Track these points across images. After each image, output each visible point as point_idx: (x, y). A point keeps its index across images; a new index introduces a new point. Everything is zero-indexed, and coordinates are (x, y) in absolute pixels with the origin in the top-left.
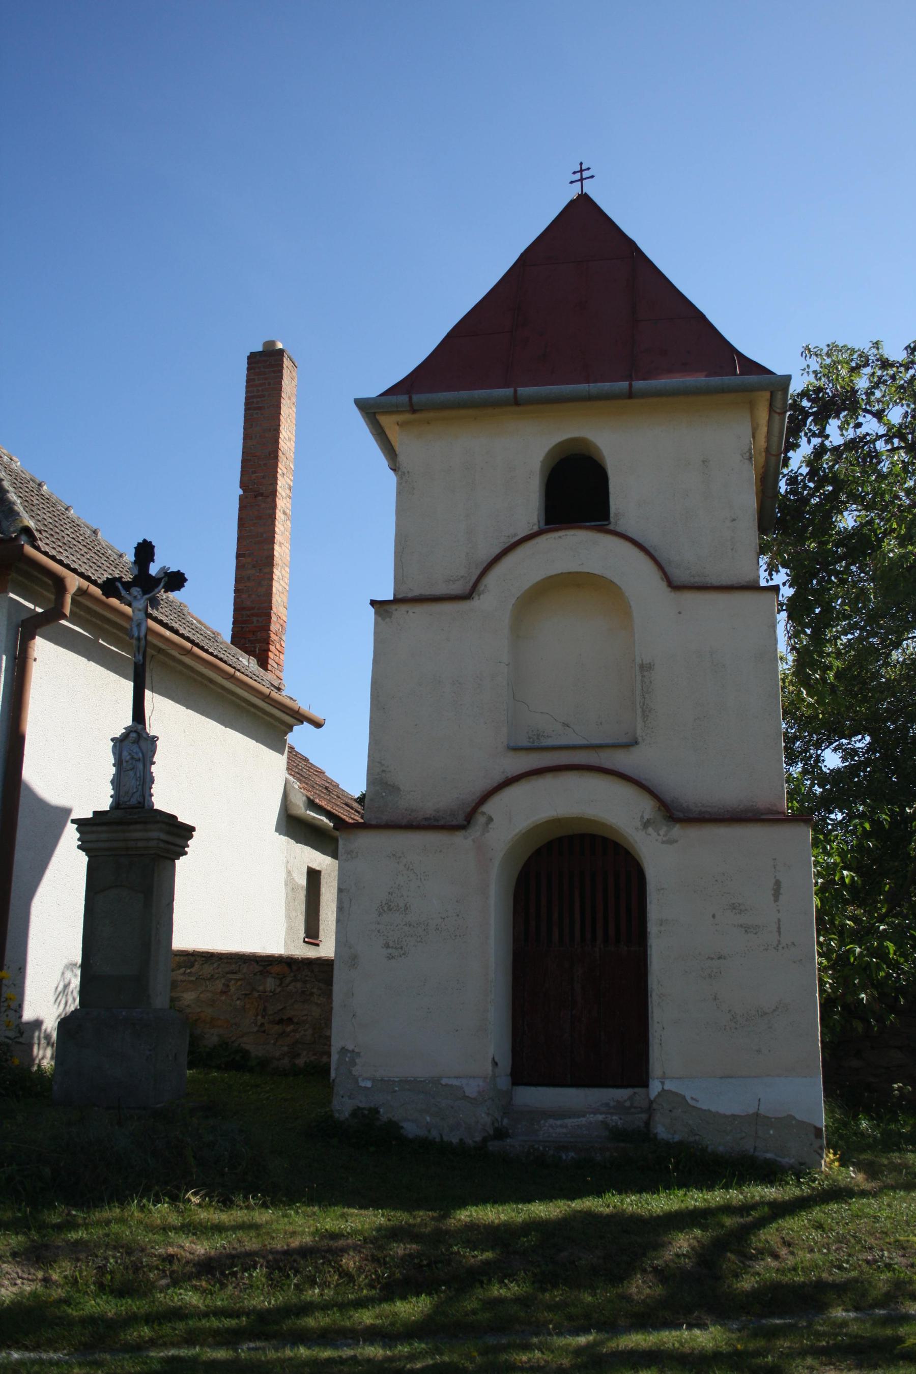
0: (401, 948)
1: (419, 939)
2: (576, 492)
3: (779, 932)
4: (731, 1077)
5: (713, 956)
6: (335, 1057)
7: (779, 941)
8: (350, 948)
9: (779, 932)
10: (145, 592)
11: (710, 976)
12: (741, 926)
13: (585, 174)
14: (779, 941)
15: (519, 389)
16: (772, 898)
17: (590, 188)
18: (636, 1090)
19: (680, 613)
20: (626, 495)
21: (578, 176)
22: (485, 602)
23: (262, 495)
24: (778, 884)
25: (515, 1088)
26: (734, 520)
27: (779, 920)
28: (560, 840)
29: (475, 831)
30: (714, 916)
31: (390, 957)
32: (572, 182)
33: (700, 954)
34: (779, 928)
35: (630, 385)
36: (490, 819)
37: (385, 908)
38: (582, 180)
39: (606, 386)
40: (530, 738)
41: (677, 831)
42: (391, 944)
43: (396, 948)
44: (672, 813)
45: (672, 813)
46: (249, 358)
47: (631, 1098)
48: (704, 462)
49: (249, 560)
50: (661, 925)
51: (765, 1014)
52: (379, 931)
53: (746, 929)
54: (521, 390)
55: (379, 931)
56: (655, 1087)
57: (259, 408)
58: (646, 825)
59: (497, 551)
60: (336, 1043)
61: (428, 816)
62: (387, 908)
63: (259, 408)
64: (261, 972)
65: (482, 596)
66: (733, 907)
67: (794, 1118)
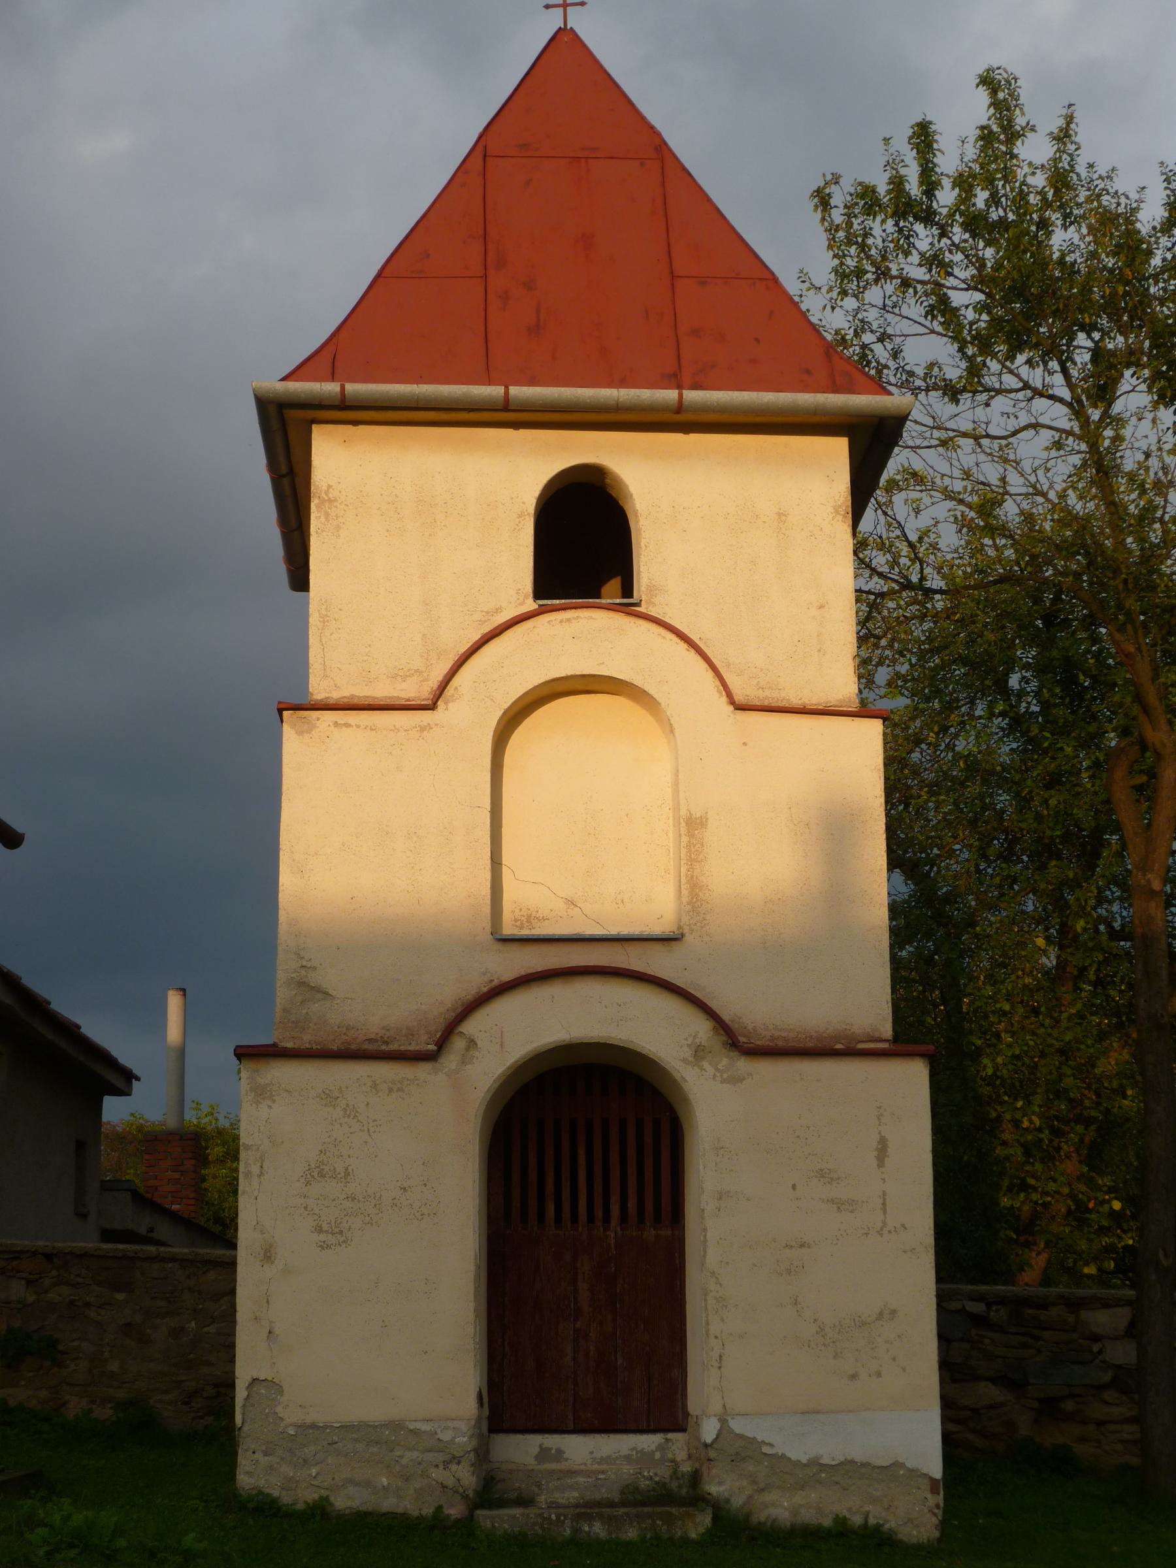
0: (341, 1232)
1: (368, 1219)
2: (583, 545)
3: (884, 1210)
4: (817, 1412)
5: (793, 1244)
6: (241, 1393)
7: (884, 1223)
8: (262, 1232)
9: (884, 1210)
11: (789, 1272)
12: (832, 1201)
14: (884, 1223)
15: (511, 388)
16: (875, 1162)
18: (670, 1436)
19: (745, 744)
20: (660, 554)
22: (447, 714)
25: (494, 1436)
26: (821, 607)
27: (884, 1193)
29: (450, 1060)
30: (794, 1187)
31: (324, 1246)
32: (547, 7)
33: (774, 1240)
34: (884, 1204)
35: (681, 396)
36: (472, 1043)
37: (315, 1174)
39: (645, 395)
40: (516, 920)
41: (744, 1064)
42: (325, 1227)
43: (333, 1234)
44: (737, 1041)
45: (737, 1041)
47: (661, 1448)
48: (779, 514)
50: (720, 1199)
51: (864, 1324)
52: (306, 1208)
53: (839, 1205)
54: (514, 391)
55: (306, 1208)
56: (709, 1430)
58: (699, 1053)
60: (244, 1373)
61: (372, 1036)
62: (318, 1172)
65: (450, 705)
66: (821, 1174)
67: (902, 1465)
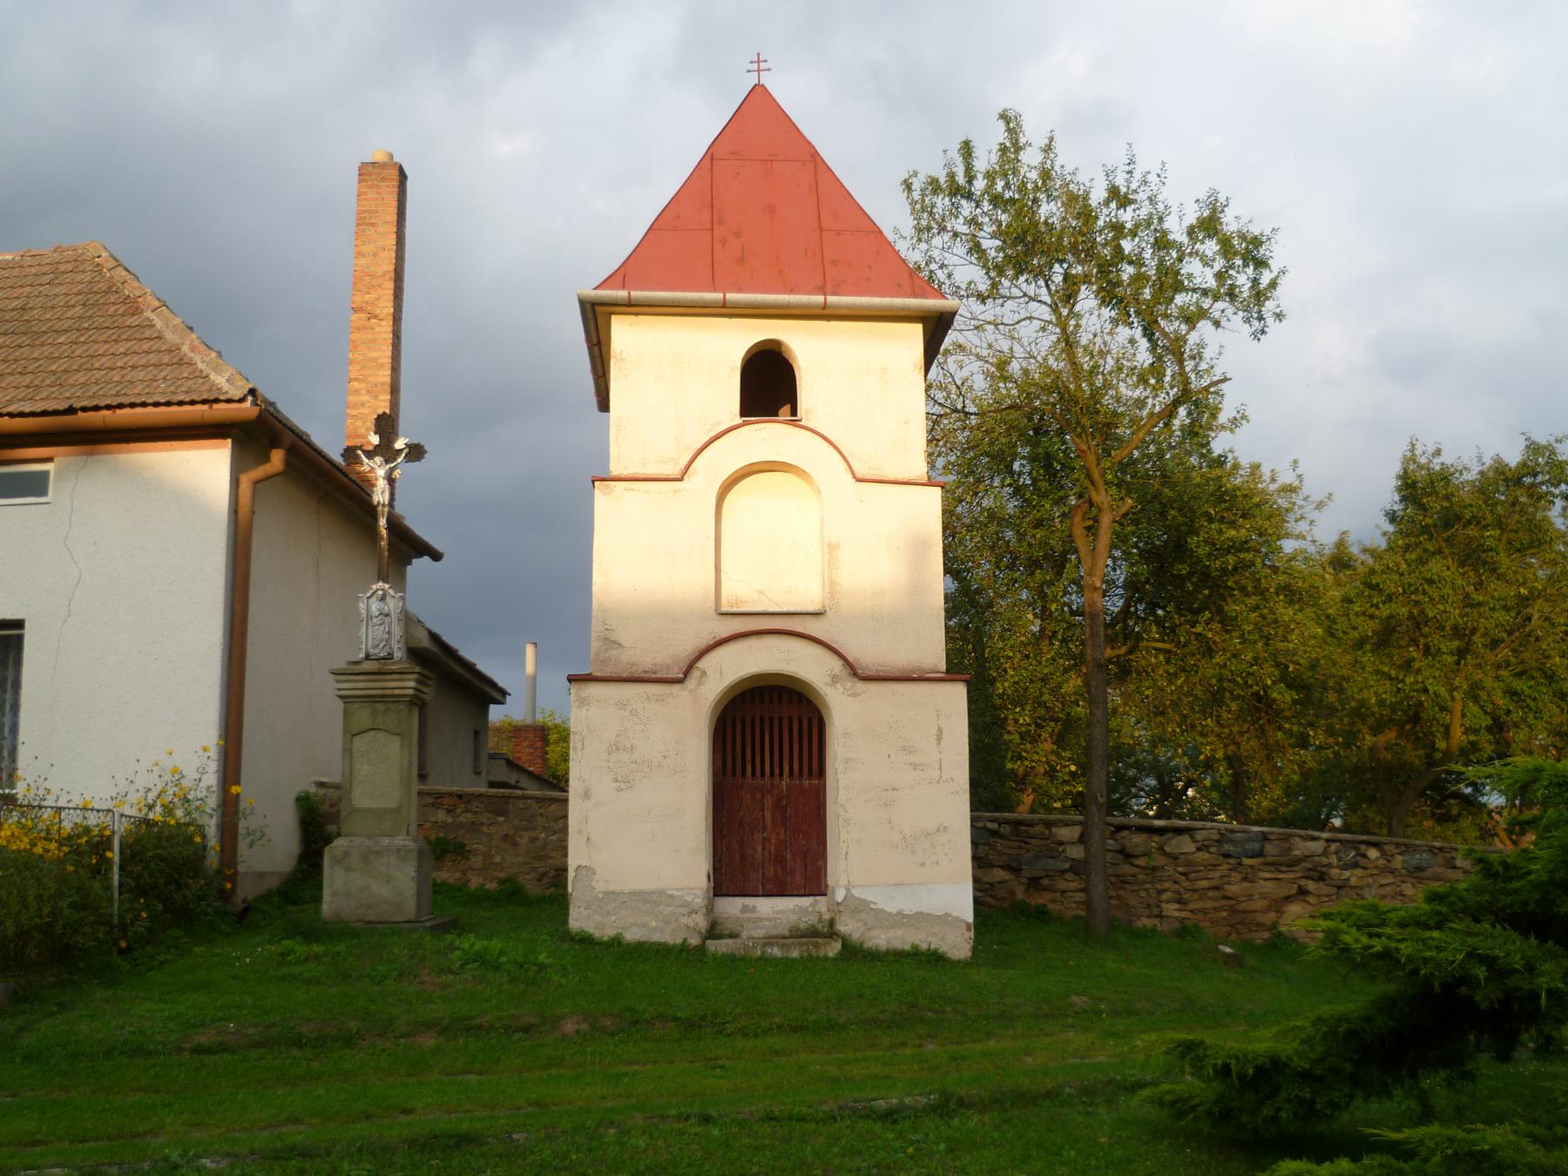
2: (768, 385)
10: (387, 462)
13: (763, 65)
17: (766, 80)
21: (755, 66)
23: (375, 317)
24: (940, 729)
28: (753, 690)
29: (691, 683)
31: (619, 790)
38: (759, 71)
44: (856, 673)
45: (856, 673)
46: (360, 169)
49: (363, 385)
53: (914, 766)
56: (840, 895)
57: (373, 224)
59: (706, 439)
62: (615, 748)
63: (373, 224)
64: (433, 805)
